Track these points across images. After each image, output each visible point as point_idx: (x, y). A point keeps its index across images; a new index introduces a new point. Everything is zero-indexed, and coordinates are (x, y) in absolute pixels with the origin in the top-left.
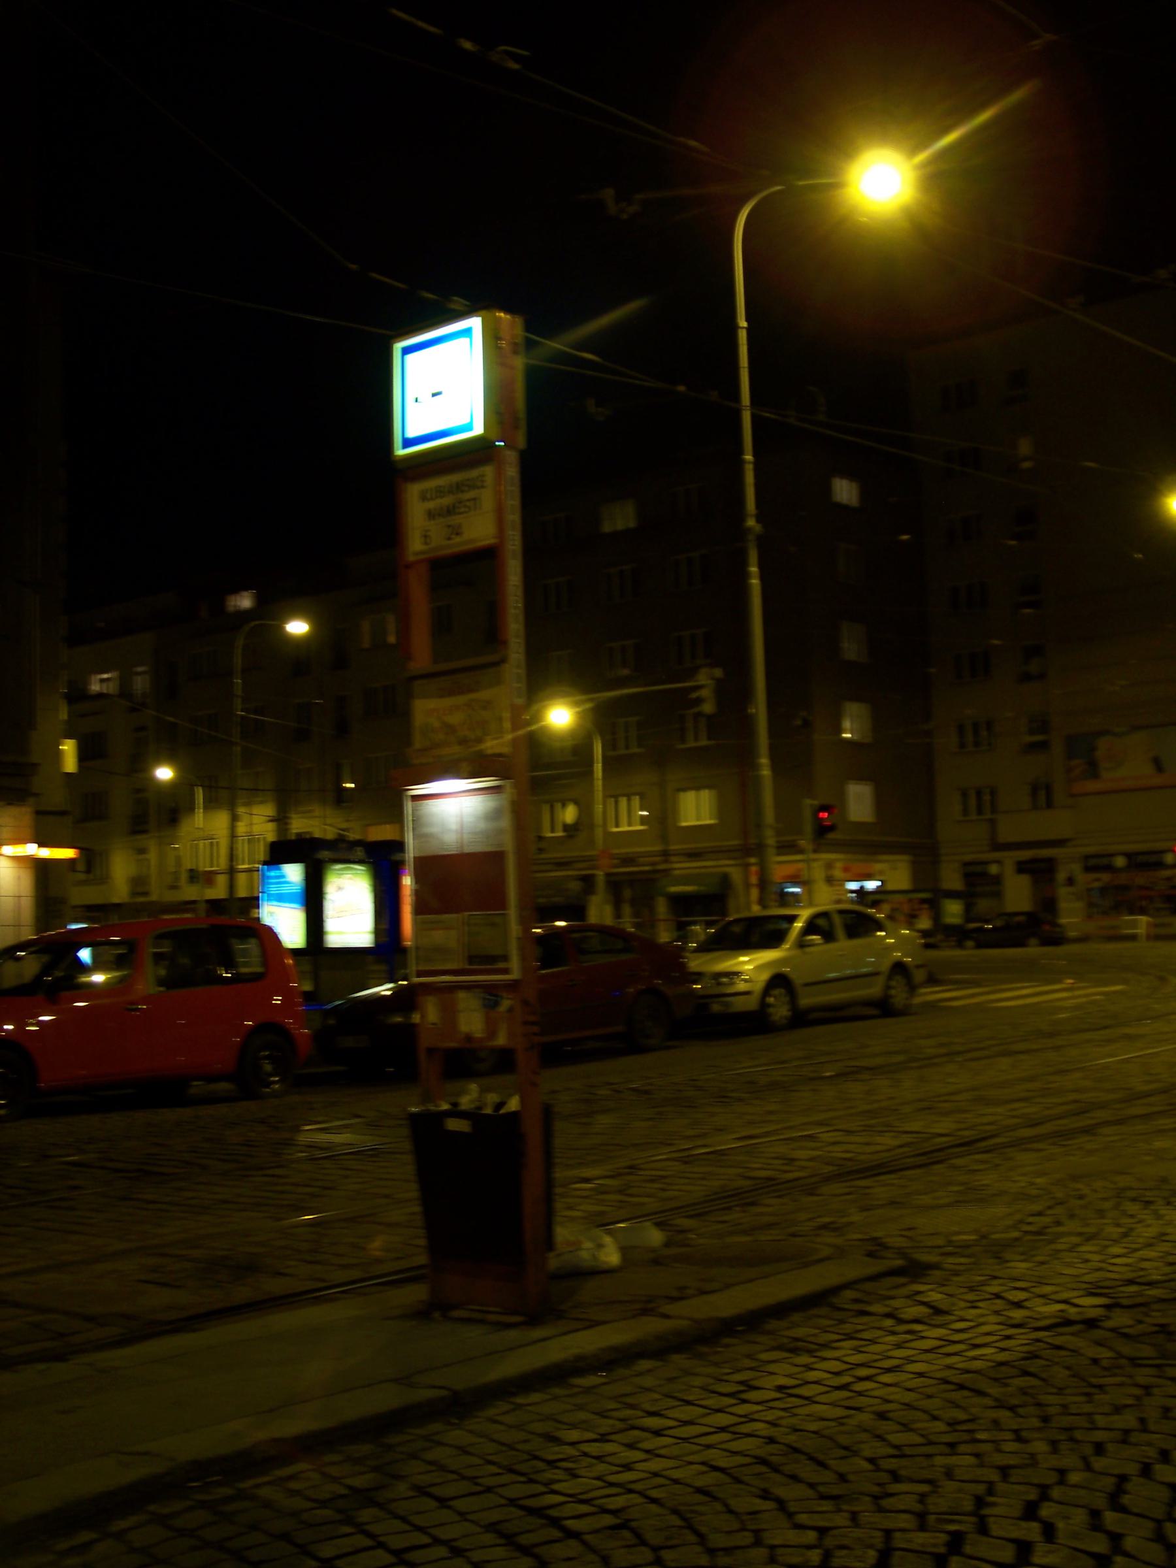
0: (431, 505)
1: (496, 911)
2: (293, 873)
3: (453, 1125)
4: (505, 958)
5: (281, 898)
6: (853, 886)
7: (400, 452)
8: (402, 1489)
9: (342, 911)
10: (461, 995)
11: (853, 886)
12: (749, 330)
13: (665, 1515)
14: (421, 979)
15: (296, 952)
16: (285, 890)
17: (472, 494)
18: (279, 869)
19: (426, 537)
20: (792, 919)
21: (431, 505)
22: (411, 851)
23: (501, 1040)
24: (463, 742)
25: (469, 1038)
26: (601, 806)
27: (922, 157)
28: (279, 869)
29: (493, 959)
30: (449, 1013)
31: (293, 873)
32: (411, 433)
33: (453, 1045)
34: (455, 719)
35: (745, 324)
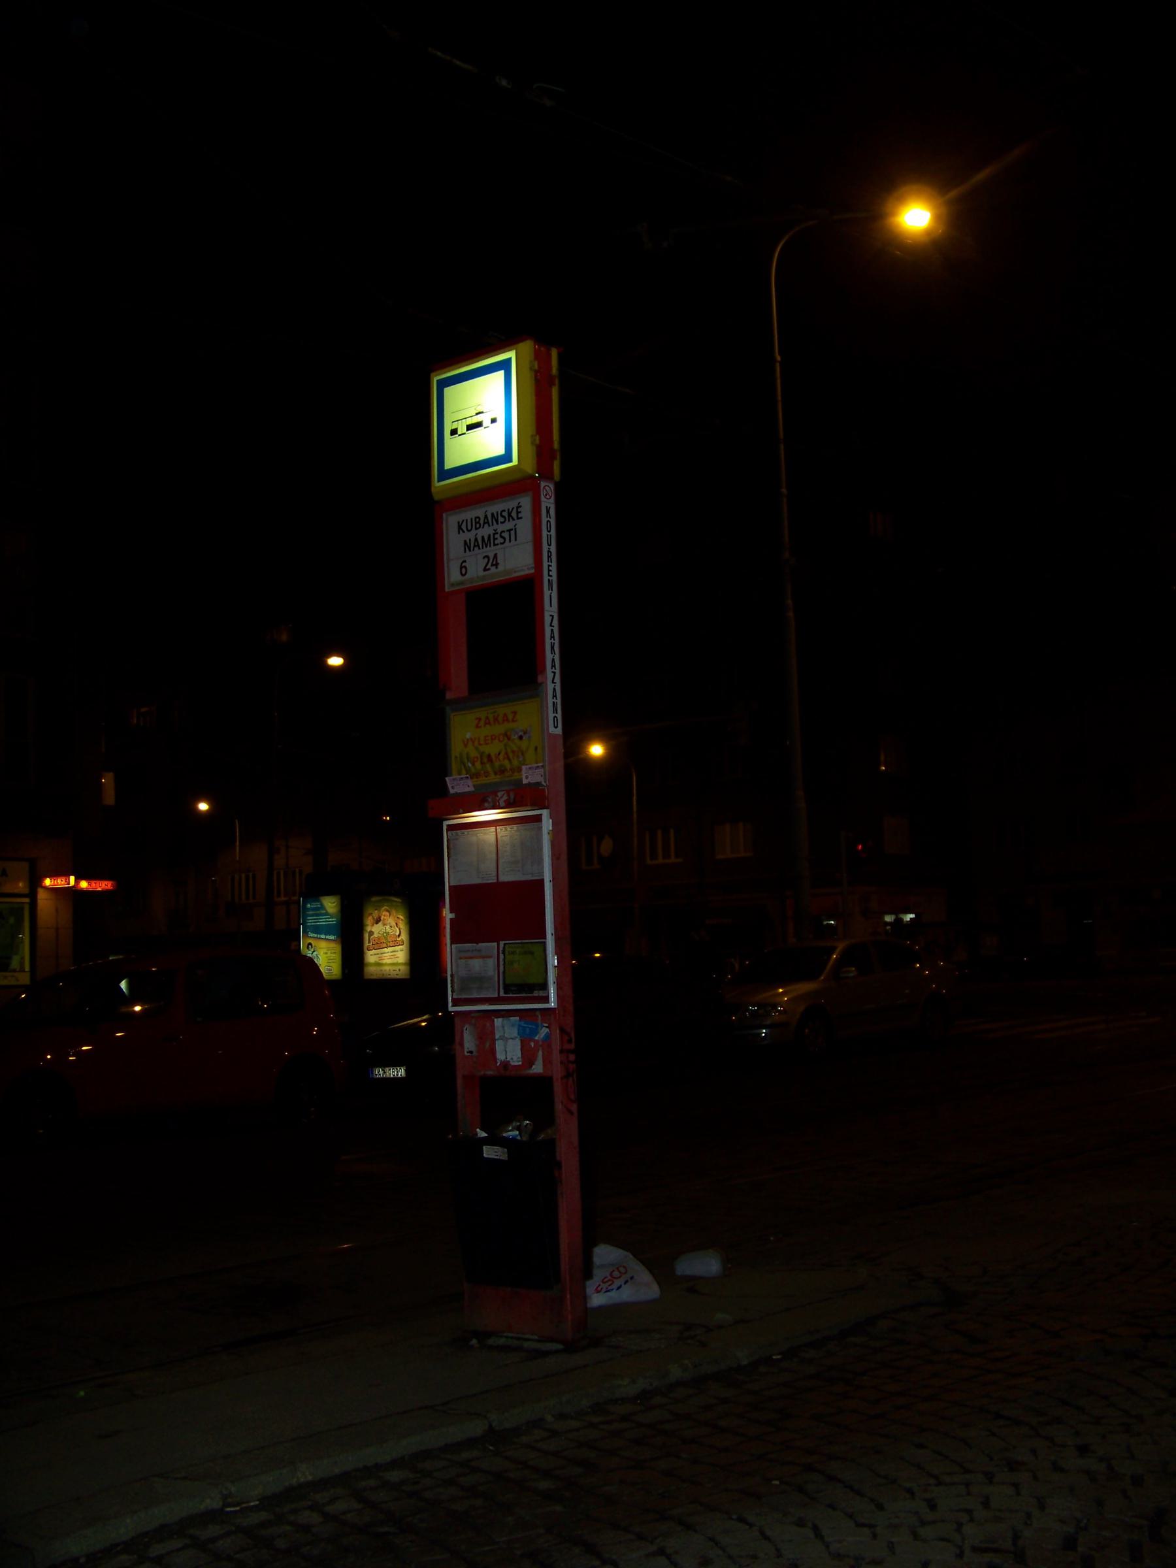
0: (470, 536)
1: (776, 270)
2: (331, 904)
3: (489, 1152)
4: (544, 986)
5: (317, 930)
6: (889, 918)
7: (437, 484)
8: (518, 951)
9: (375, 954)
10: (498, 1022)
11: (889, 918)
12: (781, 363)
13: (609, 1286)
14: (554, 419)
15: (332, 983)
16: (322, 921)
17: (509, 525)
18: (319, 901)
19: (463, 568)
20: (832, 950)
21: (470, 536)
22: (450, 879)
23: (538, 1068)
24: (502, 771)
25: (505, 1064)
26: (128, 1521)
27: (953, 194)
28: (319, 901)
29: (531, 988)
30: (486, 1037)
31: (331, 904)
32: (449, 464)
33: (490, 1073)
34: (493, 749)
35: (779, 358)
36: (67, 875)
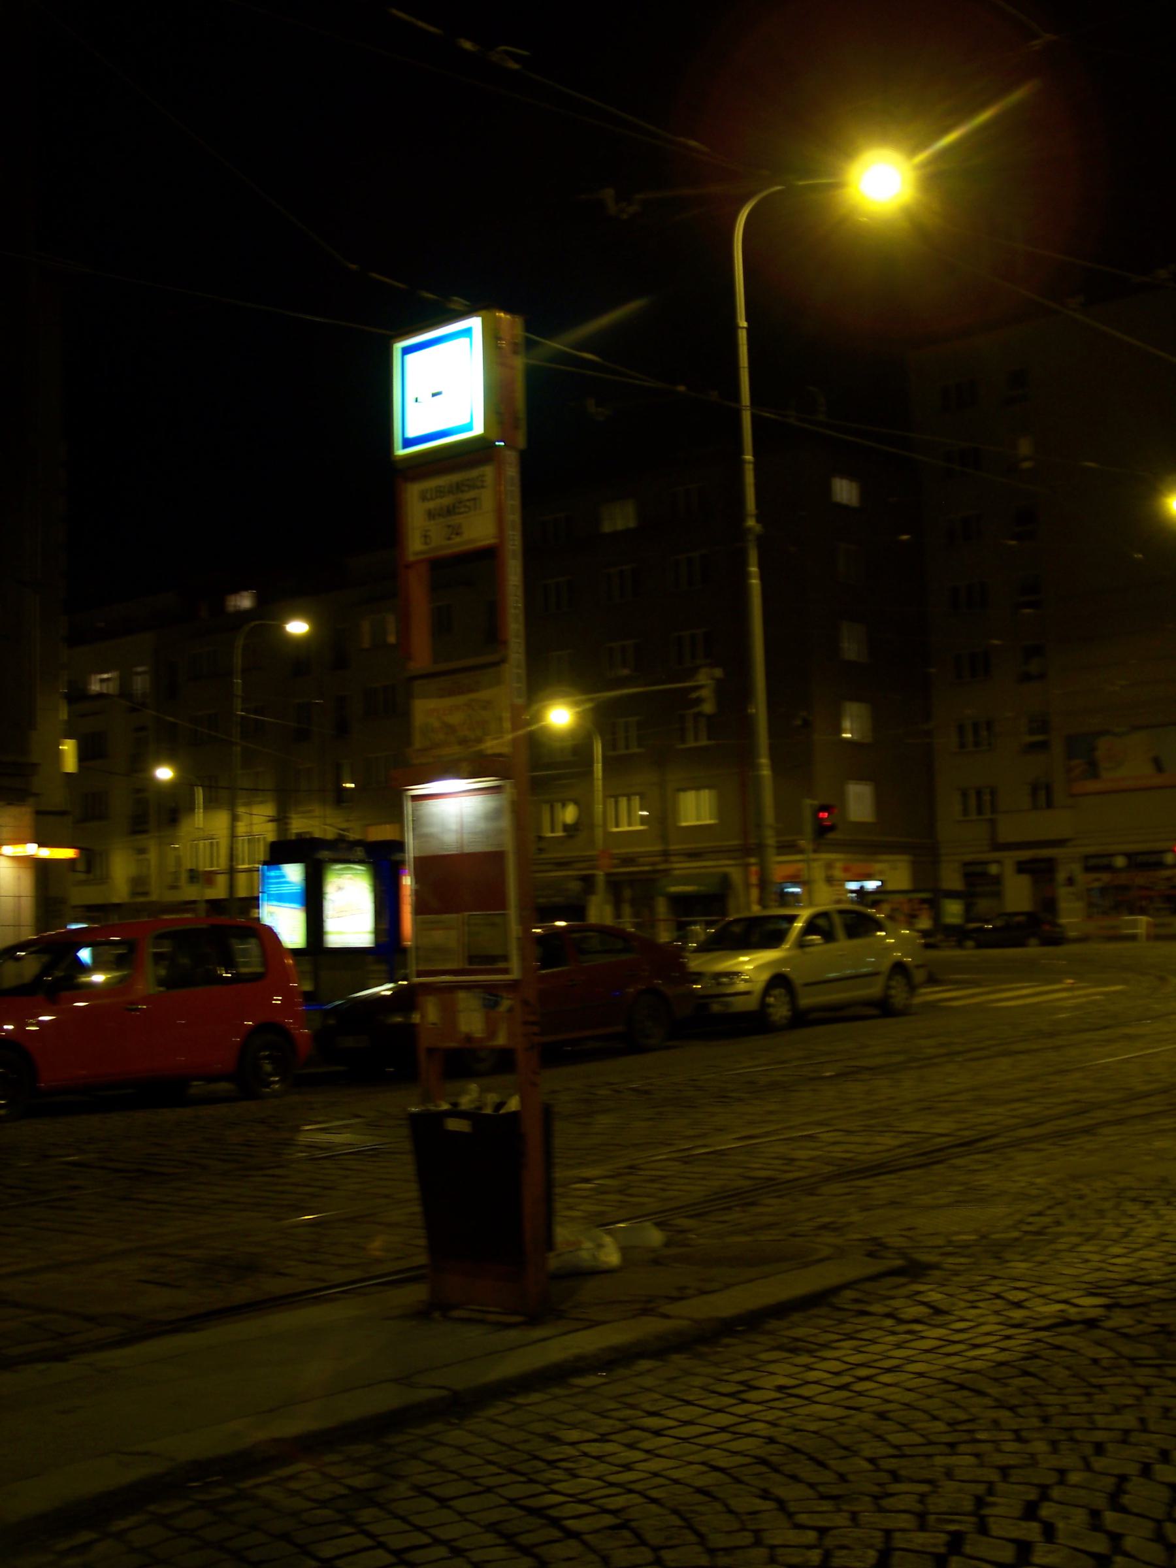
0: (431, 505)
2: (293, 873)
3: (453, 1125)
4: (505, 958)
5: (281, 898)
6: (853, 886)
7: (400, 452)
9: (342, 911)
10: (461, 995)
11: (853, 886)
12: (749, 330)
14: (421, 979)
15: (296, 952)
16: (285, 890)
17: (472, 494)
18: (279, 869)
19: (426, 537)
20: (792, 919)
21: (431, 505)
22: (411, 851)
23: (501, 1040)
24: (463, 742)
25: (469, 1038)
27: (922, 157)
28: (279, 869)
29: (493, 959)
30: (449, 1013)
31: (293, 873)
32: (411, 433)
33: (453, 1045)
34: (455, 719)
35: (745, 324)
36: (747, 320)
